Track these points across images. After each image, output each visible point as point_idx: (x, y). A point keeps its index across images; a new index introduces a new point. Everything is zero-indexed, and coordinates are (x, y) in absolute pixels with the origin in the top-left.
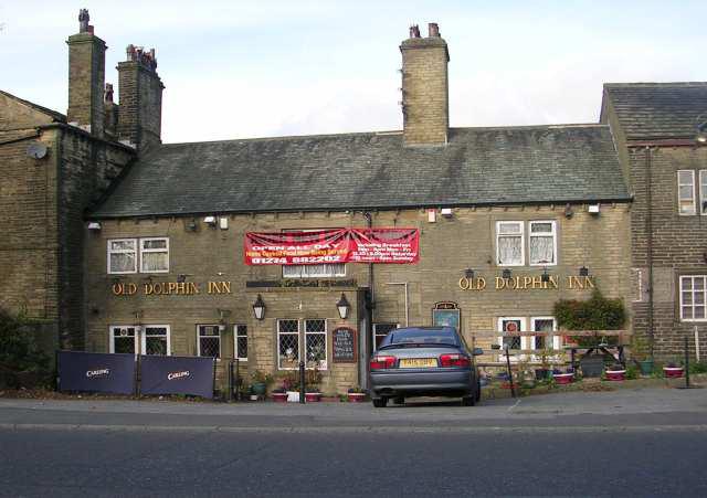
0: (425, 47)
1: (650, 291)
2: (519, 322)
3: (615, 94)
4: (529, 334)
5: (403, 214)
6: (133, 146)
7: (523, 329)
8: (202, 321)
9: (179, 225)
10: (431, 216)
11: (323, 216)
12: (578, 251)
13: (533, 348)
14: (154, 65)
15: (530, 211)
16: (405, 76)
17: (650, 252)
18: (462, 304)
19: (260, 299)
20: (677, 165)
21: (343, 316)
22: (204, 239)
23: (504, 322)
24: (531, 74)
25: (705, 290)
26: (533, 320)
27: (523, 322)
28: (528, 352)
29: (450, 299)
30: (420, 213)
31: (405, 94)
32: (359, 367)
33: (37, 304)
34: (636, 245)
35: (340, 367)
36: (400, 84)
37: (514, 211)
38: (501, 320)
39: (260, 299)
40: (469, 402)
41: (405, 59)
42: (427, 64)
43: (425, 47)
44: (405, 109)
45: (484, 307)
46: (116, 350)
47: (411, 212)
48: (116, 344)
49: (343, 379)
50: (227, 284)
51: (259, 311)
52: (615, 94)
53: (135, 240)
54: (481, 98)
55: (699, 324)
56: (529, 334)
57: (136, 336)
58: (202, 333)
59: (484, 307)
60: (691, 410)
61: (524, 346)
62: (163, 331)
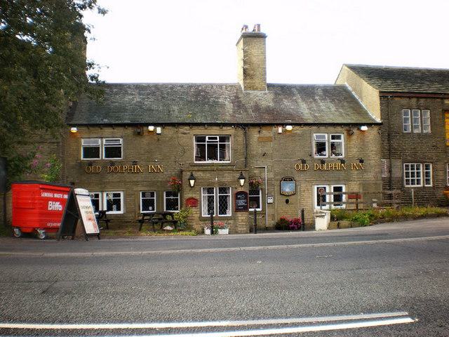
0: (255, 37)
1: (390, 172)
2: (325, 188)
4: (330, 194)
5: (264, 128)
7: (327, 191)
8: (143, 189)
9: (130, 131)
10: (280, 130)
11: (218, 128)
12: (355, 150)
13: (333, 201)
15: (331, 129)
17: (389, 150)
18: (296, 178)
19: (192, 175)
20: (402, 107)
21: (192, 185)
22: (145, 140)
23: (318, 188)
24: (309, 57)
26: (332, 187)
27: (327, 187)
28: (330, 203)
29: (290, 175)
30: (274, 129)
31: (245, 62)
33: (427, 174)
35: (239, 214)
37: (322, 128)
38: (316, 187)
39: (192, 175)
40: (299, 229)
43: (253, 38)
47: (268, 128)
48: (143, 202)
49: (240, 221)
50: (161, 166)
51: (192, 182)
53: (100, 140)
54: (283, 68)
55: (413, 188)
56: (330, 194)
57: (100, 199)
58: (143, 196)
61: (327, 201)
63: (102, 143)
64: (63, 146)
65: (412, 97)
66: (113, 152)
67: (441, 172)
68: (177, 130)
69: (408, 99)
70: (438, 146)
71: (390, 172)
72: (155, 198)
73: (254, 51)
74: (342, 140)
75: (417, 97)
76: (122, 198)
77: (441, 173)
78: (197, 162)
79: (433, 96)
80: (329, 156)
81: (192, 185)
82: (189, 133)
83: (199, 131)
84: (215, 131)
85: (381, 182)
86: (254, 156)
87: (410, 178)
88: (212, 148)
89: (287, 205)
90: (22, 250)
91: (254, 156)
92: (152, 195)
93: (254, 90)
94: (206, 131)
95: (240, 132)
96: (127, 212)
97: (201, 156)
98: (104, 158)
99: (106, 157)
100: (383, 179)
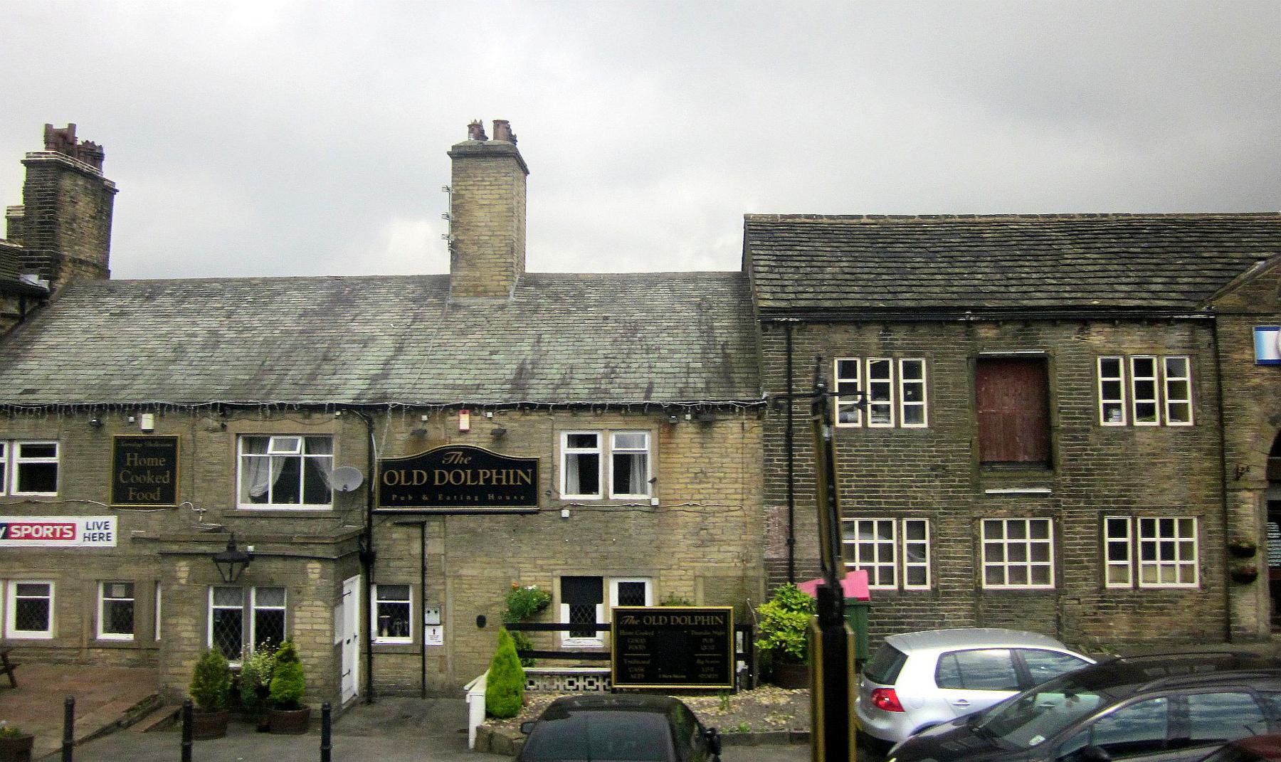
1: (791, 543)
3: (762, 233)
6: (44, 284)
14: (94, 154)
16: (456, 197)
17: (790, 481)
25: (410, 602)
31: (454, 225)
32: (815, 749)
34: (768, 471)
36: (447, 209)
41: (456, 172)
42: (489, 179)
44: (453, 247)
45: (539, 562)
46: (129, 631)
52: (762, 233)
59: (539, 562)
60: (344, 663)
62: (45, 589)
64: (159, 410)
65: (867, 323)
67: (960, 547)
69: (852, 329)
70: (950, 466)
71: (791, 543)
73: (485, 195)
75: (882, 322)
77: (959, 550)
78: (1147, 357)
79: (935, 316)
85: (762, 572)
87: (1158, 539)
89: (481, 634)
90: (544, 665)
93: (478, 295)
95: (358, 427)
96: (61, 636)
99: (21, 489)
100: (769, 564)
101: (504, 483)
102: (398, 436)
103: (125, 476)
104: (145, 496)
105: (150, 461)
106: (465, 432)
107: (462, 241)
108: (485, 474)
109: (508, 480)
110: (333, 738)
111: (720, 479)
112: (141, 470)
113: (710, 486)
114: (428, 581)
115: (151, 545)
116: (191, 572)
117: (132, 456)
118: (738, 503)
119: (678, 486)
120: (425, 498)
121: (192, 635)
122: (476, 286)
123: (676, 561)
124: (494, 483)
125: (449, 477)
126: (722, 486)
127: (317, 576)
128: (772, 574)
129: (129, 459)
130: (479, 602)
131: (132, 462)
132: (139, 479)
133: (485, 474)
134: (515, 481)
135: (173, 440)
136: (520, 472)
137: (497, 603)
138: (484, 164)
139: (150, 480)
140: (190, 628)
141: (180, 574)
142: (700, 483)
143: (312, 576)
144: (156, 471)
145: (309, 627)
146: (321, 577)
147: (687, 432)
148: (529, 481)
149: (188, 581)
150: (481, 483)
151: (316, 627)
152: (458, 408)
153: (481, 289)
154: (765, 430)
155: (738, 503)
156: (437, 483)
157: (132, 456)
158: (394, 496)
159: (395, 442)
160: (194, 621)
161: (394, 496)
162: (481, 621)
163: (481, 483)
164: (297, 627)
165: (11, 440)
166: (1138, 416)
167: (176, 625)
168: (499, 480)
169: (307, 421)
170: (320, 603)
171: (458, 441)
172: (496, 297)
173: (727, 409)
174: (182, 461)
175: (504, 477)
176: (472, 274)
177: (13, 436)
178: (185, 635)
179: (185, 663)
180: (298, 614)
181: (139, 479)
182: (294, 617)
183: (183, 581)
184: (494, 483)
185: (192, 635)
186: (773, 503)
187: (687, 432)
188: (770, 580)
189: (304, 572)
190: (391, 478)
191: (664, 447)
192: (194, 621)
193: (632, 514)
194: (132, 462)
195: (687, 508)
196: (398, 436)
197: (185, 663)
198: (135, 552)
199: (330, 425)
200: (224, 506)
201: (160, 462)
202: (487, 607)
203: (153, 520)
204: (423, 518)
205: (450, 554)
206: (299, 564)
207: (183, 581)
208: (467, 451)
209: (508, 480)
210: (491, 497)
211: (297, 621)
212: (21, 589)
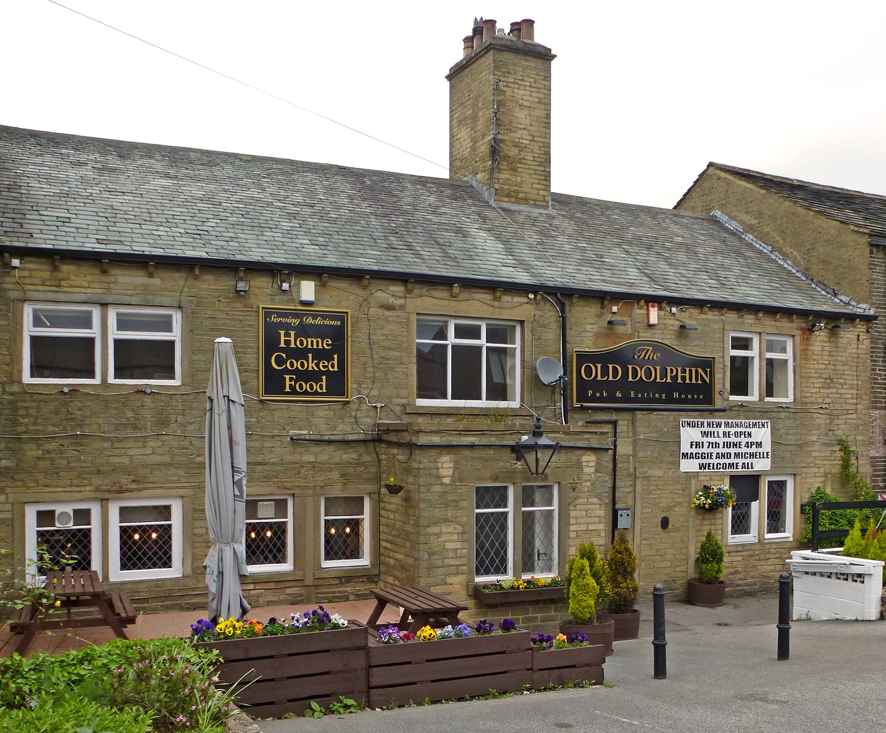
11: (487, 297)
21: (379, 622)
30: (638, 312)
63: (106, 331)
66: (137, 359)
68: (363, 293)
72: (290, 520)
74: (789, 356)
76: (176, 522)
80: (761, 399)
81: (379, 622)
82: (402, 307)
83: (432, 302)
84: (479, 307)
86: (56, 268)
88: (467, 359)
89: (663, 535)
91: (56, 268)
92: (281, 506)
94: (453, 303)
95: (549, 313)
97: (430, 386)
98: (111, 380)
101: (688, 381)
102: (588, 327)
103: (280, 361)
104: (306, 387)
105: (310, 343)
106: (651, 326)
107: (503, 141)
108: (672, 371)
109: (691, 379)
110: (670, 636)
111: (842, 384)
112: (300, 354)
113: (835, 391)
114: (618, 484)
115: (316, 449)
116: (455, 468)
117: (287, 335)
118: (853, 407)
119: (814, 390)
120: (619, 395)
121: (458, 545)
122: (518, 192)
123: (812, 460)
124: (679, 381)
125: (641, 374)
126: (843, 391)
127: (592, 470)
128: (875, 471)
129: (283, 339)
130: (664, 503)
131: (287, 342)
132: (297, 365)
133: (672, 371)
134: (697, 380)
135: (341, 317)
136: (700, 370)
137: (679, 504)
138: (524, 63)
139: (312, 366)
140: (455, 537)
141: (443, 472)
142: (828, 388)
143: (586, 470)
144: (320, 355)
145: (584, 527)
146: (596, 471)
147: (820, 336)
148: (708, 380)
149: (453, 481)
150: (669, 380)
151: (591, 527)
152: (651, 300)
153: (521, 195)
154: (872, 342)
155: (853, 407)
156: (630, 379)
157: (287, 335)
158: (590, 392)
159: (588, 331)
160: (459, 529)
161: (590, 392)
162: (665, 523)
163: (669, 380)
164: (572, 528)
165: (104, 305)
166: (746, 394)
167: (438, 535)
168: (684, 378)
169: (496, 304)
170: (595, 500)
171: (646, 335)
172: (535, 206)
173: (851, 318)
174: (355, 341)
175: (687, 375)
176: (513, 179)
177: (109, 299)
178: (449, 545)
179: (449, 580)
180: (573, 514)
181: (297, 365)
182: (569, 517)
183: (447, 481)
184: (679, 381)
185: (458, 545)
186: (876, 408)
187: (820, 336)
188: (874, 476)
189: (579, 466)
190: (589, 371)
191: (803, 355)
192: (459, 529)
193: (782, 415)
194: (287, 342)
195: (822, 411)
196: (588, 327)
197: (449, 580)
198: (296, 458)
199: (516, 308)
200: (404, 401)
201: (325, 344)
202: (669, 508)
203: (322, 417)
204: (614, 417)
205: (641, 454)
206: (573, 456)
207: (447, 481)
208: (658, 347)
209: (691, 379)
210: (676, 395)
211: (572, 521)
212: (125, 513)
